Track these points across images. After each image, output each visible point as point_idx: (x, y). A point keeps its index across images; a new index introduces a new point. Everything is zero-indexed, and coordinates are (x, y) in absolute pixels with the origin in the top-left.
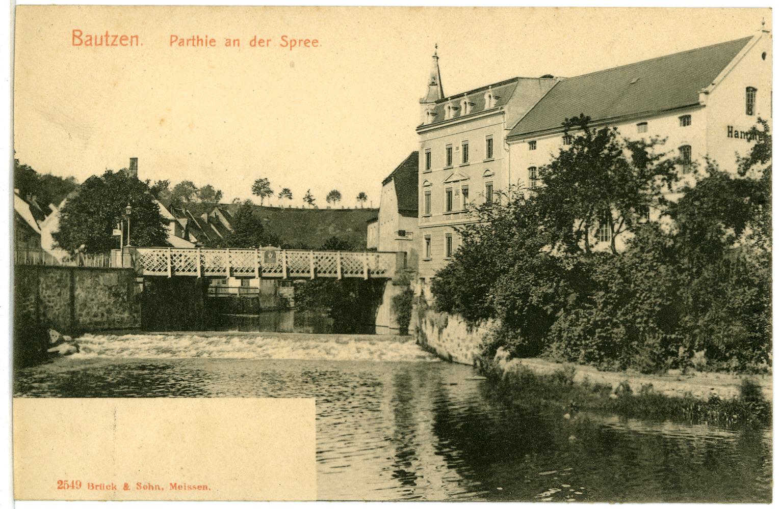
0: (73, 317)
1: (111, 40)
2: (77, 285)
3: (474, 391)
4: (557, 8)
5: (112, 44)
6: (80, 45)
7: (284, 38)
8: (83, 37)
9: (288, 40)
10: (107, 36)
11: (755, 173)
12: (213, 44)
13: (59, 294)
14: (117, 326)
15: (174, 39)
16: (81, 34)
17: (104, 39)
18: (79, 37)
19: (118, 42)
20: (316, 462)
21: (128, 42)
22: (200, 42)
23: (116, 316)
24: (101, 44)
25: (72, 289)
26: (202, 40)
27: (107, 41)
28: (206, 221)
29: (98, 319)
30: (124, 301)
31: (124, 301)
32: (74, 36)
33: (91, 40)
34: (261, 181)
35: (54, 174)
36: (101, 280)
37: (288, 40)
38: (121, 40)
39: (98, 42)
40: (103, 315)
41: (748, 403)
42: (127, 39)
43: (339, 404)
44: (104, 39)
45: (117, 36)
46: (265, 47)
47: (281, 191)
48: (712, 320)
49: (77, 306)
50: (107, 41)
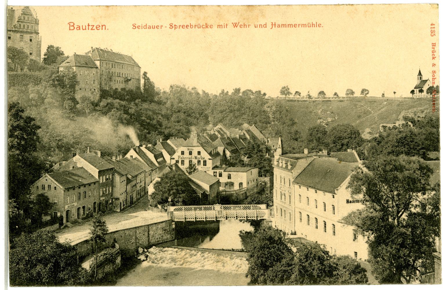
0: (149, 241)
1: (90, 27)
2: (150, 230)
4: (108, 6)
13: (144, 235)
14: (166, 241)
19: (95, 28)
20: (244, 224)
23: (165, 237)
24: (102, 26)
25: (149, 231)
28: (238, 137)
29: (159, 240)
30: (168, 231)
31: (168, 231)
34: (284, 87)
36: (159, 226)
40: (160, 238)
41: (418, 272)
47: (295, 92)
49: (150, 237)
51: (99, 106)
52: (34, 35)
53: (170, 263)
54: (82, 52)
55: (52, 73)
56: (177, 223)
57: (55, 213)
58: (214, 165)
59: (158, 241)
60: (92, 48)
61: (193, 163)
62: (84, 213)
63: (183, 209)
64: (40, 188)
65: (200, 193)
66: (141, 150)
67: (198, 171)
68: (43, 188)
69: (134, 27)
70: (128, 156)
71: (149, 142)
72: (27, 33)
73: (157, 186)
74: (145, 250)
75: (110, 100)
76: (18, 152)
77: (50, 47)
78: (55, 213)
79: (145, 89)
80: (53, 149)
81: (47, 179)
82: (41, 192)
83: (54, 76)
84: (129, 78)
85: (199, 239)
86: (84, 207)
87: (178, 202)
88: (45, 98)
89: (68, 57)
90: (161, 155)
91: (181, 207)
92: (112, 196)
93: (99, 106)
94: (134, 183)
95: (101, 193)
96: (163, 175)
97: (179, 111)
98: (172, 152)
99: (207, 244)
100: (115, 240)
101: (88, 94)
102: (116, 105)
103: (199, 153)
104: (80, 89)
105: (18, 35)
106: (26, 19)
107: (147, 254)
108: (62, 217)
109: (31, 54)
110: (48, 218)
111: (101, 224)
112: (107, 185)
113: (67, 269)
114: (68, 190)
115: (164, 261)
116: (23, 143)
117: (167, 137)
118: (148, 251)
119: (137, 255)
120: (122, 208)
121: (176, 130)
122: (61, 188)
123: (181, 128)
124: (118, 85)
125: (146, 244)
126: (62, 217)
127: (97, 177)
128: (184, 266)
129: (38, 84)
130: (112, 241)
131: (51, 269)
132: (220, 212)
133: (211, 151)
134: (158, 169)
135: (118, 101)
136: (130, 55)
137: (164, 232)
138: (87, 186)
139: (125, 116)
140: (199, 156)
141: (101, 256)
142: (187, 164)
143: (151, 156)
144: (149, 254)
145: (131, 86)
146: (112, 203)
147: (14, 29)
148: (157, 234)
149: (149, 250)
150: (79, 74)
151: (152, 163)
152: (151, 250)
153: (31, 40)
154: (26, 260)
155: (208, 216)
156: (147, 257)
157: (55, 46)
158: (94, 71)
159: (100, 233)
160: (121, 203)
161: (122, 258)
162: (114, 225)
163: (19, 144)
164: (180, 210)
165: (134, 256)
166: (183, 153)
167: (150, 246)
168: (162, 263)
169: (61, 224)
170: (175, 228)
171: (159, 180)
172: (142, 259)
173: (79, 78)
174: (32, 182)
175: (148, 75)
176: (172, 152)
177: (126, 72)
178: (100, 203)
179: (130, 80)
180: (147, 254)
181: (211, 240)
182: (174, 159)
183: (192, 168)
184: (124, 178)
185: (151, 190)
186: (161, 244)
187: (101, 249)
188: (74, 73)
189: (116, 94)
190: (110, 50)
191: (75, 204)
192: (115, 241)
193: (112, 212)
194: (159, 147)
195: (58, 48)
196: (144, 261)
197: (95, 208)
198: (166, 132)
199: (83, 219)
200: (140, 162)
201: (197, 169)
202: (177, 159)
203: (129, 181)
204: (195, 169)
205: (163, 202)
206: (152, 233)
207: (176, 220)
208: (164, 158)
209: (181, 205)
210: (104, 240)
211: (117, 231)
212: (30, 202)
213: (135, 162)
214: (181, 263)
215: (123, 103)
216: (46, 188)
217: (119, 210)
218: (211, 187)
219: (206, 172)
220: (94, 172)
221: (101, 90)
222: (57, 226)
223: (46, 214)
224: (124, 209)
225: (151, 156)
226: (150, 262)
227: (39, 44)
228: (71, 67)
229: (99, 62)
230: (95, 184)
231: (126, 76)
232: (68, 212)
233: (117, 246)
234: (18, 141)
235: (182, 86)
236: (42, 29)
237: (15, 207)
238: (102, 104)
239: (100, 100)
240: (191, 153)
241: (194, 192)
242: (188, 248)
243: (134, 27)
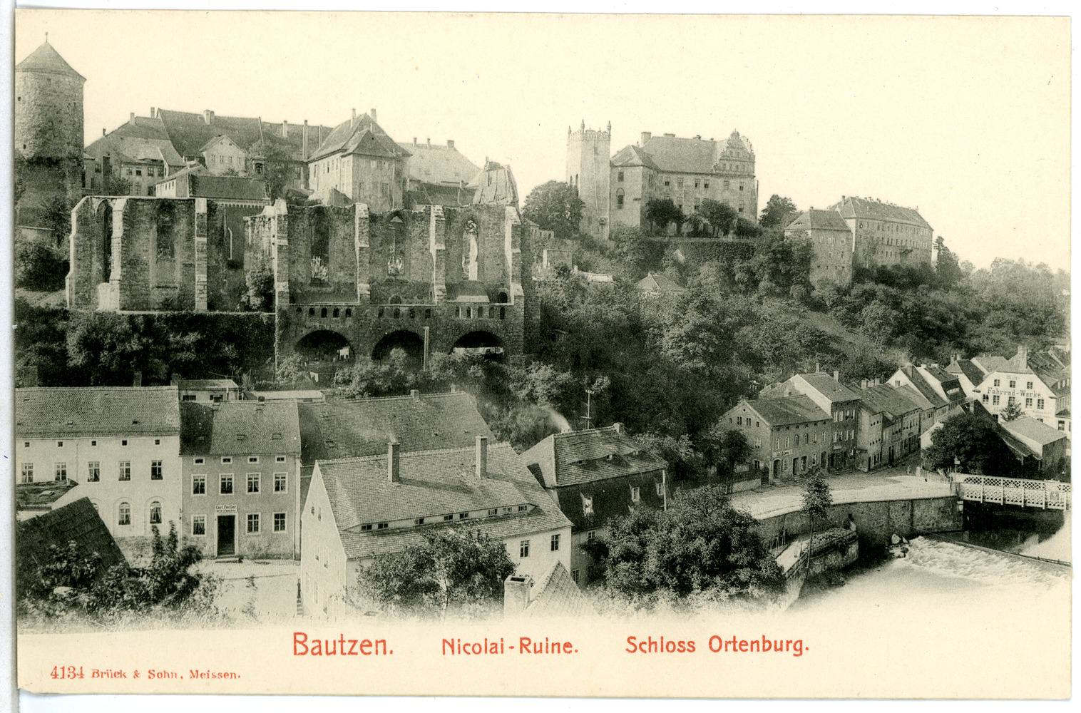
5: (350, 653)
6: (303, 654)
7: (632, 641)
9: (637, 642)
11: (796, 290)
12: (568, 649)
16: (530, 643)
17: (338, 645)
19: (357, 649)
21: (373, 649)
24: (334, 653)
25: (912, 511)
26: (655, 643)
27: (342, 648)
29: (930, 527)
32: (296, 641)
33: (496, 647)
35: (804, 172)
37: (637, 642)
39: (331, 649)
44: (338, 645)
46: (749, 652)
50: (342, 648)
51: (850, 295)
52: (747, 181)
53: (946, 568)
54: (823, 204)
55: (773, 241)
56: (967, 504)
57: (756, 462)
58: (1059, 411)
59: (929, 529)
60: (844, 197)
61: (1016, 403)
62: (804, 467)
63: (983, 480)
64: (735, 421)
65: (1021, 456)
66: (917, 372)
67: (1024, 417)
68: (740, 423)
69: (47, 34)
70: (892, 381)
71: (935, 359)
72: (734, 176)
73: (939, 435)
74: (904, 540)
75: (869, 285)
76: (702, 364)
77: (774, 198)
78: (756, 462)
79: (940, 267)
80: (765, 362)
81: (744, 409)
82: (735, 427)
83: (775, 244)
84: (909, 248)
85: (1016, 537)
86: (804, 458)
87: (974, 467)
88: (760, 281)
89: (801, 213)
90: (955, 383)
91: (979, 477)
92: (854, 445)
93: (850, 295)
94: (898, 426)
95: (836, 439)
96: (950, 419)
97: (1003, 308)
98: (977, 378)
99: (1034, 547)
100: (850, 516)
101: (833, 275)
102: (880, 294)
103: (1030, 385)
104: (819, 267)
105: (720, 181)
106: (734, 154)
107: (907, 546)
108: (766, 469)
109: (741, 210)
110: (745, 468)
111: (820, 489)
112: (845, 427)
113: (741, 551)
114: (778, 430)
115: (935, 564)
116: (711, 350)
117: (973, 352)
118: (909, 543)
119: (889, 546)
120: (873, 465)
121: (993, 340)
122: (766, 426)
123: (1002, 337)
124: (888, 259)
125: (906, 528)
126: (766, 469)
127: (829, 413)
128: (971, 577)
129: (749, 258)
130: (846, 517)
131: (717, 547)
132: (1055, 495)
133: (1056, 384)
134: (947, 407)
135: (882, 286)
136: (914, 208)
137: (941, 515)
138: (819, 424)
139: (895, 313)
140: (1029, 391)
141: (820, 540)
142: (1004, 403)
143: (935, 384)
144: (909, 548)
145: (912, 261)
146: (854, 457)
147: (714, 172)
148: (925, 516)
149: (911, 541)
150: (816, 244)
151: (936, 395)
152: (915, 541)
153: (741, 188)
154: (681, 529)
155: (1029, 499)
156: (905, 551)
157: (782, 196)
158: (843, 236)
159: (818, 502)
160: (870, 458)
161: (860, 550)
162: (843, 492)
163: (705, 352)
164: (977, 481)
165: (884, 546)
166: (997, 383)
167: (912, 535)
168: (931, 566)
169: (765, 480)
170: (964, 510)
171: (941, 426)
172: (896, 554)
173: (816, 249)
174: (722, 412)
175: (945, 243)
176: (977, 378)
177: (903, 237)
178: (833, 455)
179: (911, 251)
180: (907, 546)
181: (1040, 541)
182: (979, 392)
183: (1013, 413)
184: (879, 418)
185: (926, 441)
186: (935, 534)
187: (822, 529)
188: (808, 240)
189: (885, 277)
190: (875, 200)
191: (790, 452)
192: (851, 518)
193: (853, 469)
194: (955, 370)
195: (785, 200)
196: (899, 557)
197: (823, 462)
198: (974, 342)
199: (801, 476)
200: (914, 392)
201: (1023, 413)
202: (985, 392)
203: (886, 423)
204: (1018, 414)
205: (944, 465)
206: (919, 513)
207: (965, 497)
208: (961, 389)
209: (980, 474)
210: (824, 515)
211: (855, 503)
212: (714, 442)
213: (903, 393)
214: (967, 572)
215: (893, 291)
216: (744, 423)
217: (866, 470)
218: (1045, 447)
219: (1042, 420)
220: (824, 403)
221: (854, 268)
222: (756, 482)
223: (741, 462)
224: (875, 468)
225: (935, 384)
226: (910, 561)
227: (754, 193)
228: (801, 231)
229: (854, 220)
230: (816, 424)
231: (904, 244)
232: (776, 462)
233: (853, 526)
234: (704, 348)
235: (1017, 261)
236: (760, 170)
237: (691, 447)
238: (854, 292)
239: (852, 286)
240: (1012, 384)
241: (1013, 455)
242: (987, 549)
243: (47, 34)
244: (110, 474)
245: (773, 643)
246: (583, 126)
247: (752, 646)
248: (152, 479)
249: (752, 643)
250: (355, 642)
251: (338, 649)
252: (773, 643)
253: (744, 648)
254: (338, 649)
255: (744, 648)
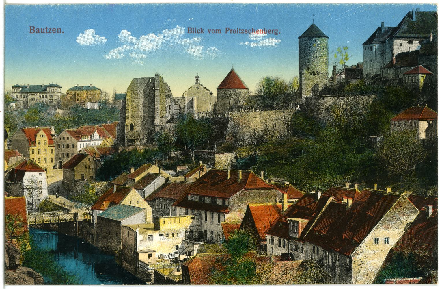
1: (48, 31)
3: (240, 220)
6: (33, 33)
8: (35, 29)
10: (46, 29)
15: (227, 29)
18: (33, 29)
19: (51, 31)
22: (254, 31)
38: (53, 30)
42: (271, 31)
43: (359, 277)
44: (45, 30)
45: (51, 29)
48: (265, 167)
244: (42, 151)
245: (196, 32)
246: (154, 252)
247: (273, 32)
248: (9, 280)
249: (58, 29)
250: (51, 29)
251: (45, 32)
252: (196, 32)
253: (270, 32)
254: (45, 32)
255: (54, 31)
